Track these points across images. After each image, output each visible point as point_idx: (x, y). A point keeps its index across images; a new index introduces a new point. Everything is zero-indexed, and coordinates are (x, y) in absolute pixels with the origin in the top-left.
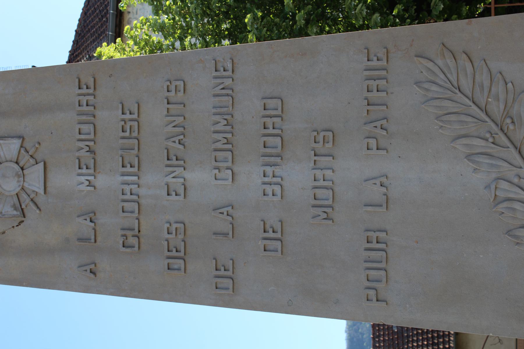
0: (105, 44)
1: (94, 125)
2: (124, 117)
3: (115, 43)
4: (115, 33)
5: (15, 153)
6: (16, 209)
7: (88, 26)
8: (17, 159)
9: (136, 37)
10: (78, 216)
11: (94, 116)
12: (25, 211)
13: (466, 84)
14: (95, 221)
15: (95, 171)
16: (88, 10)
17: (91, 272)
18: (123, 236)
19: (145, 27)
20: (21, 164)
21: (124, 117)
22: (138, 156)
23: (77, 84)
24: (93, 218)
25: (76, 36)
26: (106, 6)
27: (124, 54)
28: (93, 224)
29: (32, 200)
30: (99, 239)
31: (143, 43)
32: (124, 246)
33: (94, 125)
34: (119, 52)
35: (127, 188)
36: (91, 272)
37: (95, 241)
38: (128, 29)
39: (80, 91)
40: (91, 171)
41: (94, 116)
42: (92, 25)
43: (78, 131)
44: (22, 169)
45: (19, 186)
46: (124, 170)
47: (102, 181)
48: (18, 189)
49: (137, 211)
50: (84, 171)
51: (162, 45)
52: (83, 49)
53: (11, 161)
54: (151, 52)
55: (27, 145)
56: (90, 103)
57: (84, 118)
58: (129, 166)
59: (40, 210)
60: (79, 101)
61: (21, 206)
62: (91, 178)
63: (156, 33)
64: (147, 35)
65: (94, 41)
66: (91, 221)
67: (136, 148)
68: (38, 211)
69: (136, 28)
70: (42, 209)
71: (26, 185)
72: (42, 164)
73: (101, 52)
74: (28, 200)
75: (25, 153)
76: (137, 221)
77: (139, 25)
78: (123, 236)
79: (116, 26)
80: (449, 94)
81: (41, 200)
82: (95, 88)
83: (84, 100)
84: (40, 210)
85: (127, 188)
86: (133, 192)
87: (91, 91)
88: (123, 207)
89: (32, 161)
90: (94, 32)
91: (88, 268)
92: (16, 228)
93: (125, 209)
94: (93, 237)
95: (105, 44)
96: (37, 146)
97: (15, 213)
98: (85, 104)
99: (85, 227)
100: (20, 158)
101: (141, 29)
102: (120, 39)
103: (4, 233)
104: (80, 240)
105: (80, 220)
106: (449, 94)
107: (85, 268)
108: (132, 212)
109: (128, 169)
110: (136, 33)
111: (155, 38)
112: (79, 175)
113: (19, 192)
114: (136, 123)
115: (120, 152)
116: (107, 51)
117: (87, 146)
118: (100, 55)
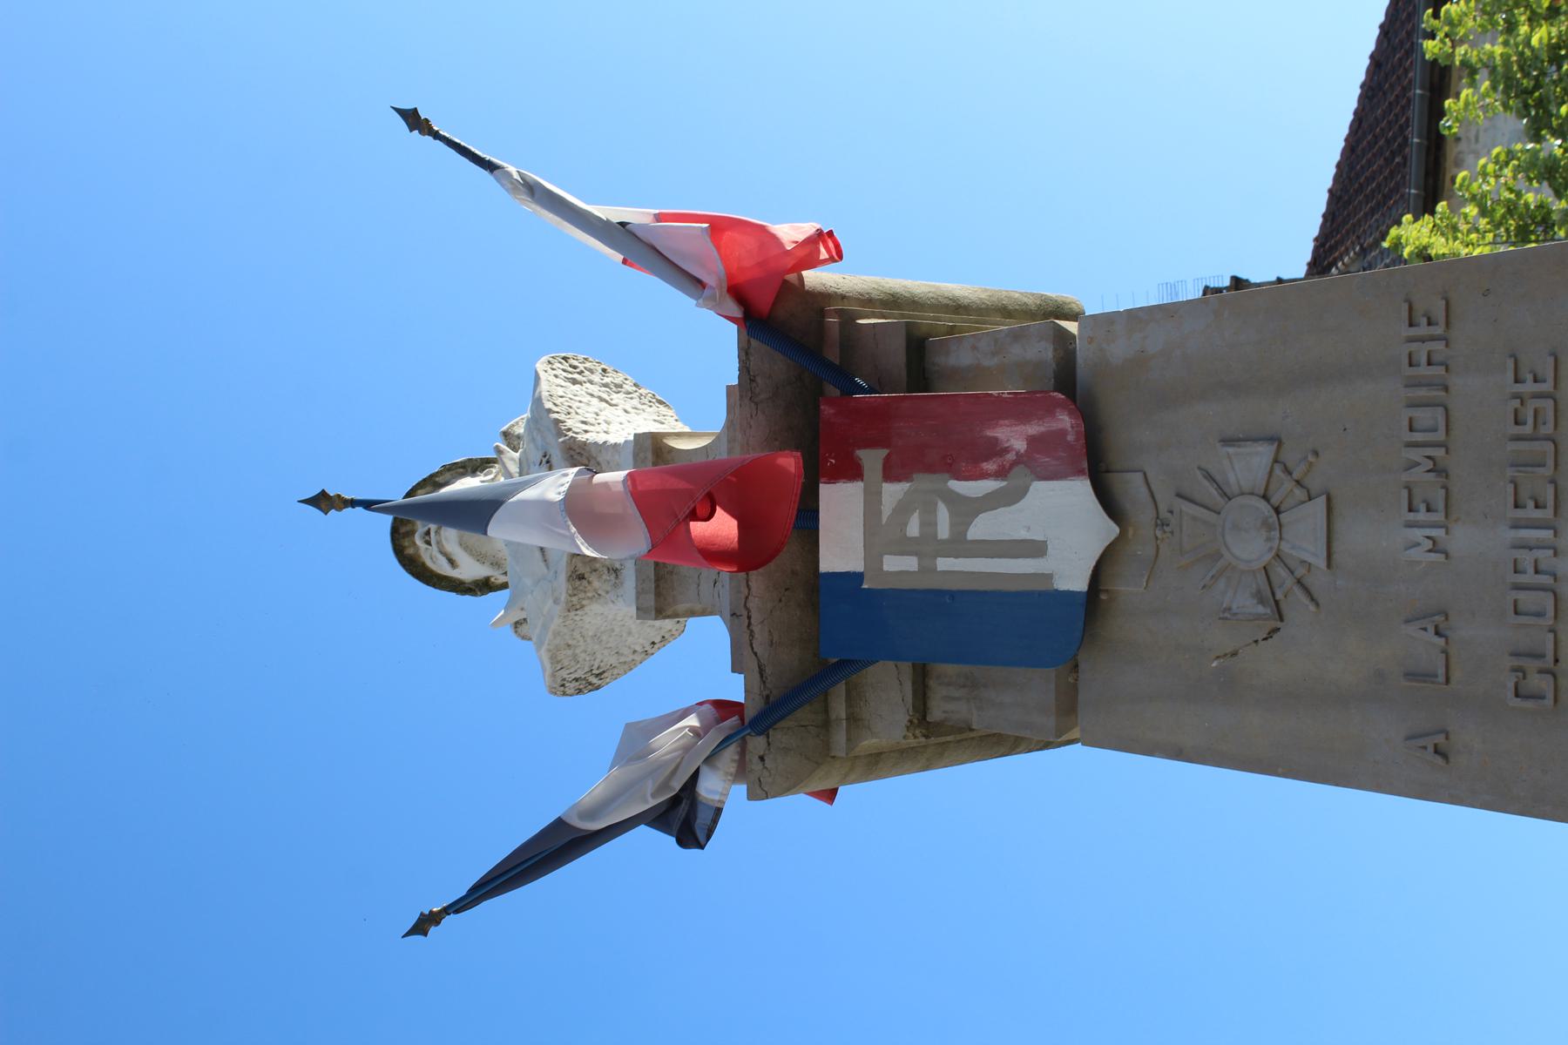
0: (1408, 217)
1: (1447, 410)
2: (1519, 388)
3: (1433, 213)
4: (1425, 190)
5: (1261, 475)
6: (1262, 601)
7: (1358, 176)
8: (1266, 489)
9: (1484, 195)
10: (1407, 621)
11: (1446, 389)
12: (1283, 606)
14: (1448, 633)
15: (1447, 516)
16: (1358, 142)
17: (1436, 752)
18: (1515, 670)
19: (1508, 172)
20: (1275, 500)
21: (1519, 388)
22: (1553, 481)
23: (1405, 314)
24: (1441, 626)
25: (1329, 203)
26: (1402, 129)
27: (1455, 239)
28: (1441, 641)
29: (1299, 581)
30: (1456, 675)
31: (1501, 211)
32: (1517, 695)
33: (1447, 410)
34: (1443, 234)
35: (1527, 558)
36: (1436, 752)
37: (1447, 681)
38: (1464, 179)
39: (1414, 332)
40: (1439, 517)
41: (1446, 389)
42: (1367, 174)
43: (1406, 423)
44: (1277, 511)
45: (1271, 549)
46: (1520, 513)
47: (1464, 538)
48: (1268, 557)
49: (1551, 613)
50: (1422, 516)
51: (1550, 212)
52: (1348, 232)
53: (1252, 494)
54: (1523, 234)
55: (1290, 456)
56: (1436, 358)
57: (1422, 393)
58: (1531, 504)
59: (1317, 605)
60: (1410, 355)
61: (1273, 594)
62: (1437, 533)
63: (1535, 184)
64: (1511, 190)
65: (1373, 211)
66: (1437, 633)
67: (1550, 463)
68: (1312, 608)
69: (1485, 175)
70: (1321, 601)
71: (1285, 547)
72: (1322, 500)
73: (1399, 238)
74: (1289, 582)
75: (1282, 475)
76: (1551, 636)
77: (1491, 168)
78: (1515, 670)
79: (1427, 174)
81: (1318, 582)
82: (1448, 324)
83: (1421, 352)
84: (1317, 605)
85: (1527, 558)
86: (1542, 566)
87: (1439, 330)
88: (1516, 601)
89: (1299, 493)
90: (1373, 191)
91: (1429, 742)
92: (1261, 643)
93: (1521, 607)
94: (1441, 671)
95: (1408, 217)
96: (1311, 458)
97: (1261, 609)
98: (1424, 360)
99: (1423, 646)
100: (1272, 487)
101: (1497, 177)
102: (1444, 203)
103: (1234, 654)
104: (1410, 675)
105: (1412, 630)
107: (1421, 742)
108: (1539, 614)
109: (1531, 512)
110: (1486, 188)
111: (1530, 197)
112: (1410, 525)
113: (1269, 563)
114: (1551, 402)
115: (1510, 472)
116: (1413, 233)
117: (1429, 457)
118: (1398, 245)
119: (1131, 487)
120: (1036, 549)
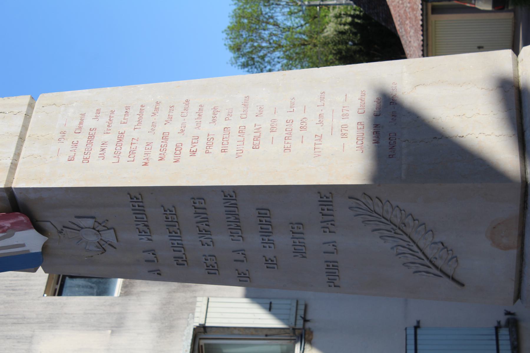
6: (98, 248)
13: (378, 210)
71: (102, 238)
80: (369, 213)
99: (151, 256)
103: (92, 256)
106: (369, 213)
119: (47, 226)
120: (23, 245)
